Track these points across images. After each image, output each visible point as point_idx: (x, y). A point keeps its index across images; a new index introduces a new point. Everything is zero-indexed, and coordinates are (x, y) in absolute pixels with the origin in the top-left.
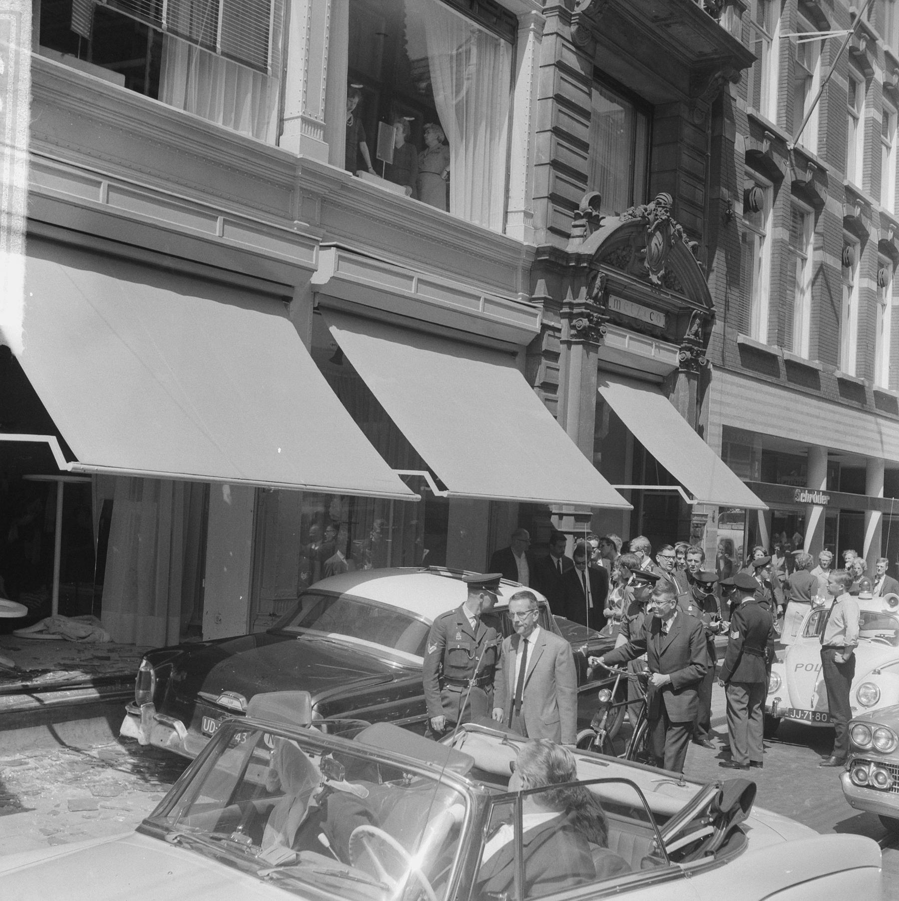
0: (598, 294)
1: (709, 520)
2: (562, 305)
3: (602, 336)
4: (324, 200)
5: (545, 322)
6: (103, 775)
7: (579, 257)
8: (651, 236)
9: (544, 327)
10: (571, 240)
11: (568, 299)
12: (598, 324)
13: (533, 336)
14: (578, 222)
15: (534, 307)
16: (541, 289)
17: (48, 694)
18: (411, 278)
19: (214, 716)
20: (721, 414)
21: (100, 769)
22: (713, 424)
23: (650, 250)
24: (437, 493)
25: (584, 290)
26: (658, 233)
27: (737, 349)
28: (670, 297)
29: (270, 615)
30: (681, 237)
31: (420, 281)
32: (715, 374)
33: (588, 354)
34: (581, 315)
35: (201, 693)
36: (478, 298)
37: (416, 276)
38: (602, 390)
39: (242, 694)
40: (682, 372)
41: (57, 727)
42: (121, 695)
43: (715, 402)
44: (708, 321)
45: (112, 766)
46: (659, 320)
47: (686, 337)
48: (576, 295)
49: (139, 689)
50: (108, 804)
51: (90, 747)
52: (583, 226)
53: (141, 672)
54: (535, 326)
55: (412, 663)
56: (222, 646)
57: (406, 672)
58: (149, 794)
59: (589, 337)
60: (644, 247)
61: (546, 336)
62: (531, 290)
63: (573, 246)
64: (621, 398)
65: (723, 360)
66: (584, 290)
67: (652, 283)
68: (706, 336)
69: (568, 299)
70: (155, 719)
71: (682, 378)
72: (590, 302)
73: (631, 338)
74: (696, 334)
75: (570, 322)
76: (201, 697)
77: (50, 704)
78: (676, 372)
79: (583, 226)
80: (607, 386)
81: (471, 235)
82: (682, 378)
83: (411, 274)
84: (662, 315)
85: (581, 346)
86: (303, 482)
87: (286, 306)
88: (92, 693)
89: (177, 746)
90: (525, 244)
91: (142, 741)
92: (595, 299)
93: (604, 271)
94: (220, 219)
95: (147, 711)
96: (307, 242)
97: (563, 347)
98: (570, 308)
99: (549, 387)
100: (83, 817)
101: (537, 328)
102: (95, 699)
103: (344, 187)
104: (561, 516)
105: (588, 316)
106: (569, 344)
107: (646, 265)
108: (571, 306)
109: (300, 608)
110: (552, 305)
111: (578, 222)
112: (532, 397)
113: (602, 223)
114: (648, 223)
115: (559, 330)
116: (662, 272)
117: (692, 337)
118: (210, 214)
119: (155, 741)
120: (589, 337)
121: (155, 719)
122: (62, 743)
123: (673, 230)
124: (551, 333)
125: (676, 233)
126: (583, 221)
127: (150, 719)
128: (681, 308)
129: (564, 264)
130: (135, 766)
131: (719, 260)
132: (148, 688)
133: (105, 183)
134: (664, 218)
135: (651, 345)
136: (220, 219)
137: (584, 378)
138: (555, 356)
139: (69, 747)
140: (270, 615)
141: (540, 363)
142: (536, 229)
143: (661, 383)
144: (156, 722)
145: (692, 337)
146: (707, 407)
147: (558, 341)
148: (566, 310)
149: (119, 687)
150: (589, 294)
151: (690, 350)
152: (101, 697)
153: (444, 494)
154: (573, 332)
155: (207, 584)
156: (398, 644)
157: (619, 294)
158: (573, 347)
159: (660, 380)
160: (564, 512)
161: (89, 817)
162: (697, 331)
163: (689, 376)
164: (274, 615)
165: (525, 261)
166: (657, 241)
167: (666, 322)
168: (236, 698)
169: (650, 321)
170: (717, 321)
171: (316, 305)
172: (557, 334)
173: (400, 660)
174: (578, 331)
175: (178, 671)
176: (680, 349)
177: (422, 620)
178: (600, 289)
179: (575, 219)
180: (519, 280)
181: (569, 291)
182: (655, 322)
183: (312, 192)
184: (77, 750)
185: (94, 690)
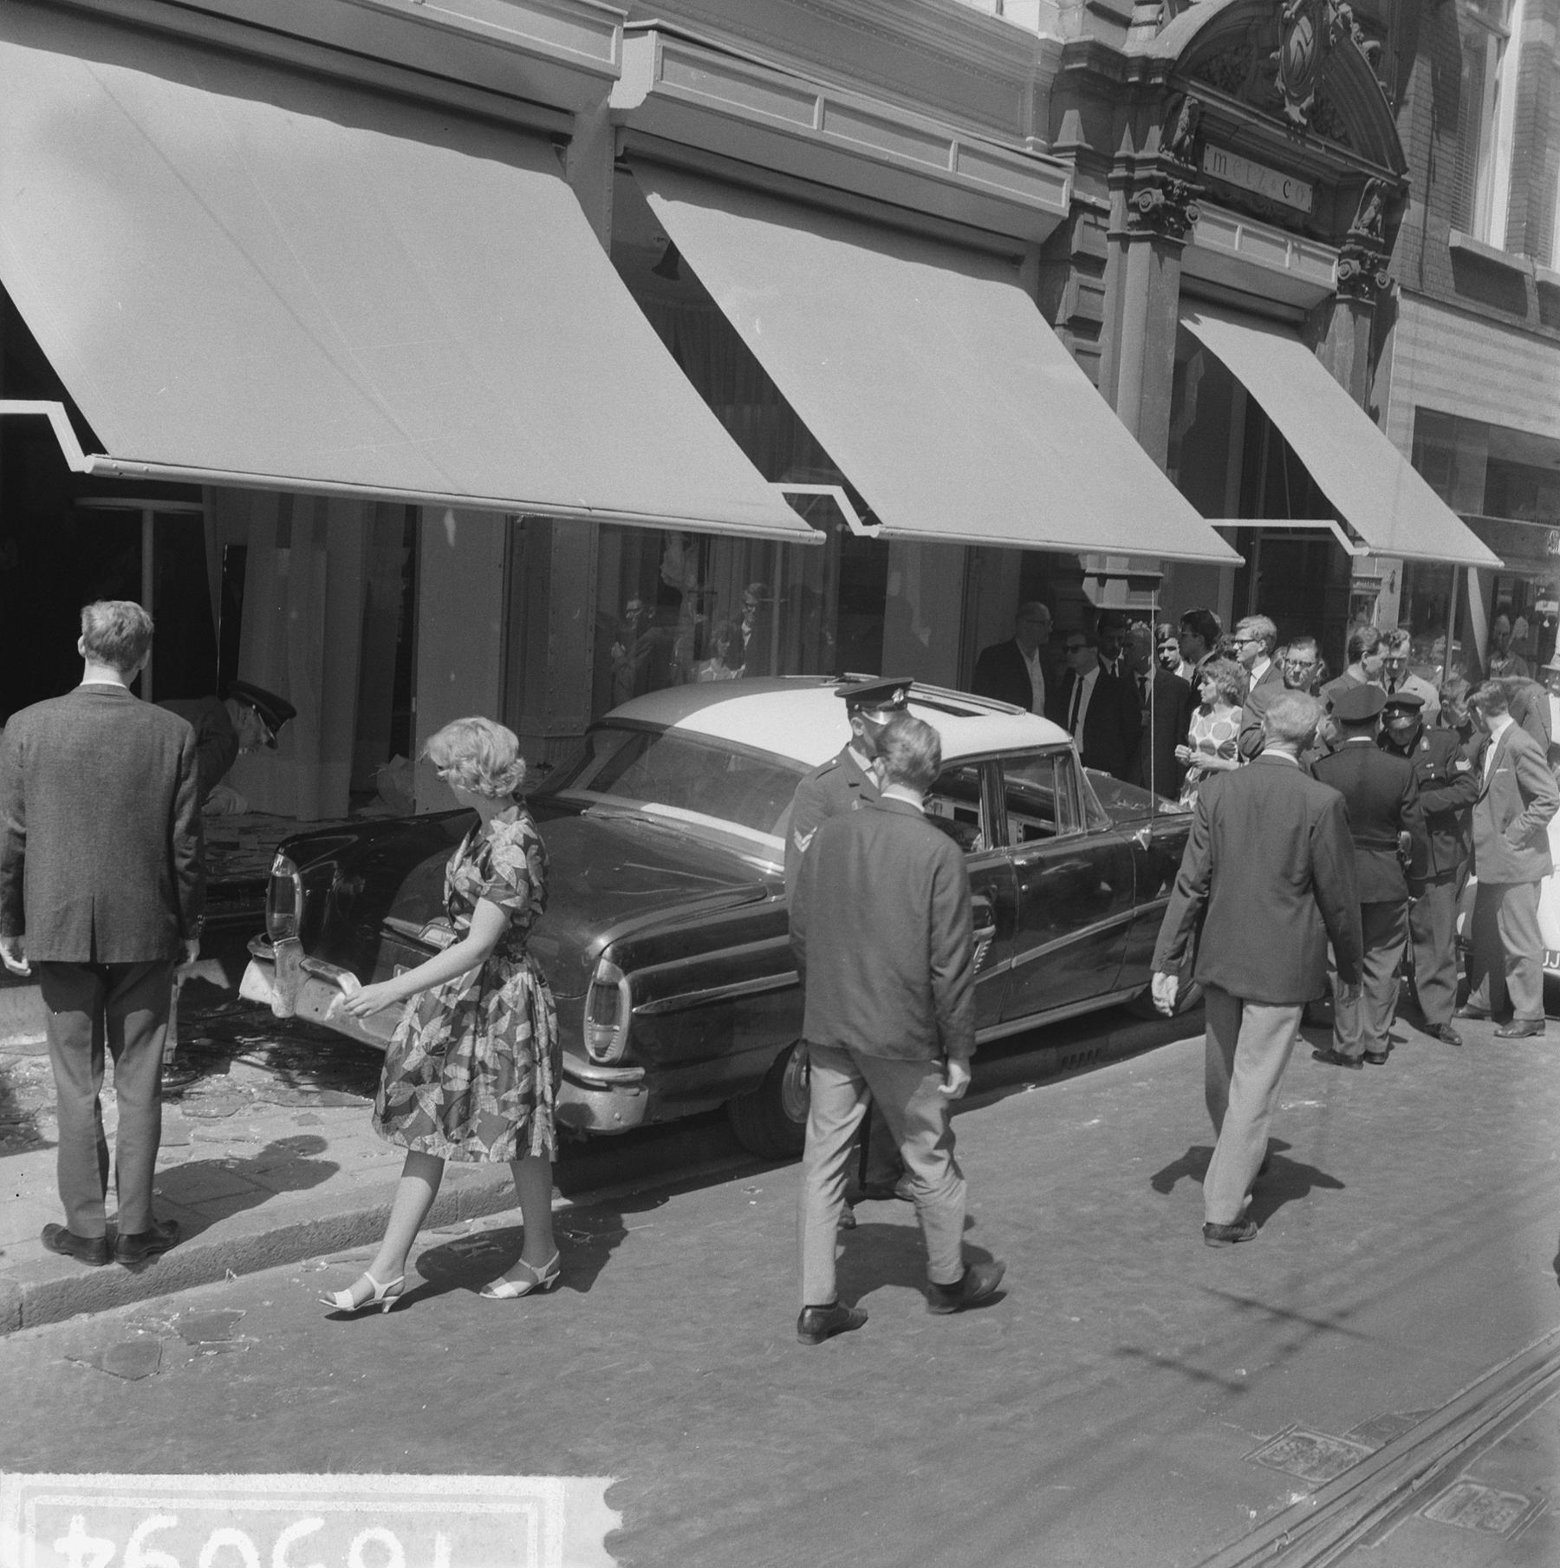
0: (1183, 139)
1: (1384, 589)
2: (1111, 163)
3: (1189, 226)
5: (1079, 195)
7: (1147, 65)
8: (1289, 25)
9: (1077, 206)
10: (1131, 30)
12: (1183, 200)
13: (1052, 226)
16: (1071, 131)
18: (811, 99)
20: (1412, 385)
23: (1288, 52)
24: (857, 527)
25: (1155, 133)
26: (1304, 20)
27: (1448, 258)
28: (1323, 151)
30: (1349, 30)
31: (829, 105)
32: (1405, 306)
33: (1161, 260)
34: (1150, 182)
35: (390, 920)
36: (946, 143)
37: (822, 95)
40: (1341, 301)
43: (1402, 360)
44: (1394, 201)
46: (1300, 198)
47: (1352, 231)
48: (1139, 144)
59: (1164, 228)
60: (1276, 49)
62: (1052, 130)
63: (1136, 43)
66: (1155, 133)
67: (1290, 122)
68: (1391, 230)
71: (1342, 311)
72: (1168, 156)
74: (1372, 226)
75: (1128, 196)
76: (390, 928)
78: (1330, 300)
82: (1342, 311)
83: (811, 89)
84: (1307, 187)
86: (584, 503)
90: (1042, 36)
92: (1178, 150)
93: (1196, 94)
97: (1113, 247)
98: (1127, 169)
99: (1082, 328)
101: (1062, 207)
104: (1102, 579)
105: (1163, 184)
106: (1124, 240)
108: (1130, 163)
110: (1092, 161)
116: (1310, 100)
117: (1364, 232)
119: (304, 1011)
120: (1164, 228)
121: (304, 969)
123: (1332, 14)
125: (1339, 21)
128: (1343, 174)
129: (1118, 78)
132: (288, 907)
135: (1284, 246)
141: (1067, 279)
143: (1301, 321)
144: (304, 976)
148: (1119, 172)
151: (1359, 256)
153: (873, 531)
154: (1133, 216)
158: (1132, 245)
159: (1296, 316)
160: (1108, 571)
163: (1356, 308)
165: (1039, 71)
167: (1314, 202)
169: (1282, 199)
170: (1412, 203)
171: (620, 154)
172: (1101, 221)
174: (1142, 214)
175: (348, 875)
176: (1340, 257)
178: (1188, 131)
181: (1127, 135)
182: (1291, 202)
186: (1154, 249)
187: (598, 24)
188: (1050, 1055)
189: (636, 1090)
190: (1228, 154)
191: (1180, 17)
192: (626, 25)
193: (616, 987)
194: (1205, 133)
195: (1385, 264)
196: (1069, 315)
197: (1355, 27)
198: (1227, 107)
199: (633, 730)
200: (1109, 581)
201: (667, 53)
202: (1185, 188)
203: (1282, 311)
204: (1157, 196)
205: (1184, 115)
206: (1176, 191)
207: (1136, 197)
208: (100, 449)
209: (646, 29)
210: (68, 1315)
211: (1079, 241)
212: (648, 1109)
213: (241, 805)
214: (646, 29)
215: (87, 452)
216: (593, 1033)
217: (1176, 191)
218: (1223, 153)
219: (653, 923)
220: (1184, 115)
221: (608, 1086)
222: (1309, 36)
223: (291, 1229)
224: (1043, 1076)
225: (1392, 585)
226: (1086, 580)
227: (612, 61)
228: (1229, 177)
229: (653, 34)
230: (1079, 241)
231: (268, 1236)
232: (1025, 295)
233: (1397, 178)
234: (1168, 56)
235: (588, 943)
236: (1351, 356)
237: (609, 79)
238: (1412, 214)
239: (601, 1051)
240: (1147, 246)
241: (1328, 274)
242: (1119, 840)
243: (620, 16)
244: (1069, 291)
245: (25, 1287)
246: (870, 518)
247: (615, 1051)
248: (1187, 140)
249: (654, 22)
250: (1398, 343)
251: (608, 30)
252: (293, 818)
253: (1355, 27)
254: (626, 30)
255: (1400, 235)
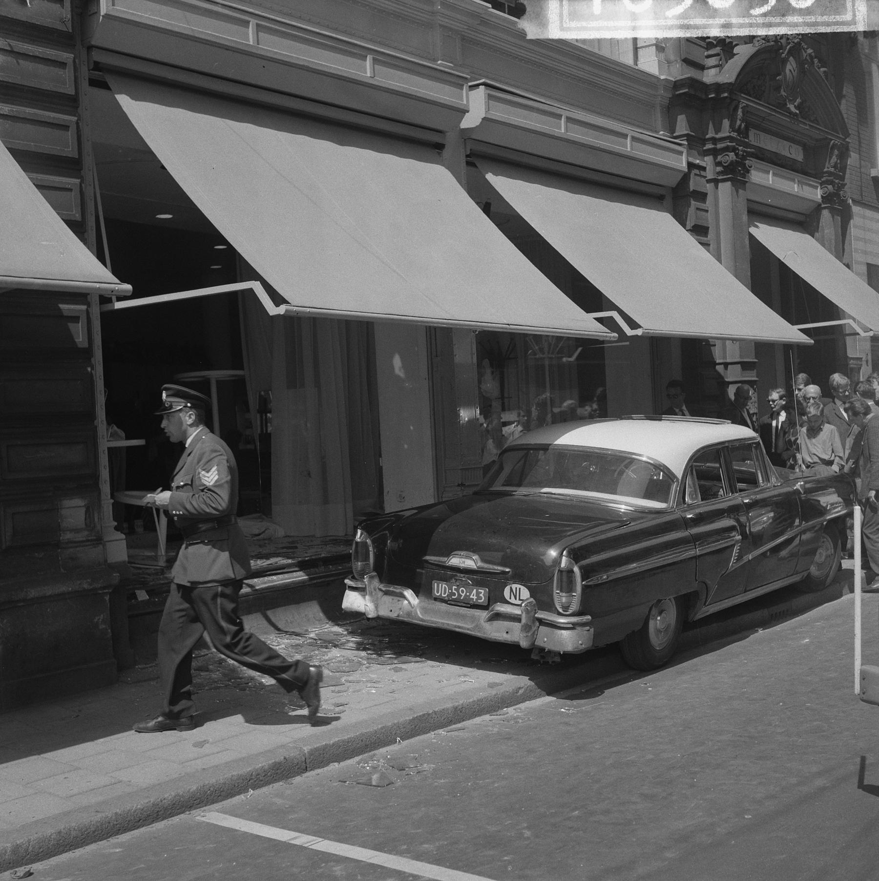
0: (740, 125)
1: (864, 363)
2: (704, 141)
3: (748, 171)
4: (463, 38)
5: (691, 160)
6: (330, 655)
7: (718, 87)
8: (784, 61)
9: (690, 165)
10: (705, 71)
11: (710, 135)
12: (744, 158)
13: (679, 177)
14: (711, 52)
15: (680, 145)
16: (682, 126)
17: (256, 580)
18: (559, 117)
19: (445, 579)
20: (865, 253)
21: (325, 650)
22: (858, 263)
23: (785, 76)
24: (629, 332)
25: (726, 123)
26: (791, 58)
27: (871, 183)
28: (807, 127)
29: (459, 485)
30: (813, 63)
31: (569, 119)
32: (856, 209)
33: (737, 192)
34: (727, 149)
35: (427, 558)
36: (625, 136)
37: (565, 114)
38: (752, 230)
39: (474, 552)
40: (825, 208)
41: (269, 613)
42: (321, 577)
43: (858, 239)
44: (844, 154)
45: (336, 646)
46: (797, 154)
47: (826, 170)
48: (718, 130)
49: (358, 561)
50: (351, 678)
51: (307, 631)
52: (718, 55)
53: (357, 543)
54: (682, 164)
55: (642, 507)
56: (425, 514)
57: (640, 515)
58: (389, 667)
59: (736, 173)
60: (779, 74)
61: (692, 176)
62: (672, 130)
63: (710, 77)
64: (768, 235)
65: (862, 195)
66: (726, 123)
67: (791, 113)
68: (843, 169)
69: (710, 135)
70: (380, 590)
71: (826, 213)
72: (734, 135)
73: (774, 174)
74: (835, 167)
75: (715, 158)
76: (427, 561)
77: (263, 589)
78: (818, 208)
79: (718, 55)
80: (757, 227)
81: (607, 69)
82: (826, 213)
83: (559, 111)
84: (800, 148)
85: (729, 183)
86: (505, 322)
87: (439, 154)
88: (300, 576)
89: (409, 614)
90: (662, 77)
91: (371, 615)
92: (739, 131)
93: (744, 101)
94: (369, 58)
95: (372, 582)
96: (458, 82)
97: (709, 187)
98: (713, 144)
99: (699, 231)
100: (333, 692)
101: (684, 166)
102: (303, 582)
103: (484, 22)
104: (726, 365)
105: (734, 150)
106: (716, 182)
107: (783, 93)
108: (714, 140)
109: (501, 468)
110: (695, 142)
111: (711, 52)
112: (689, 240)
113: (736, 50)
114: (781, 47)
115: (704, 169)
116: (799, 100)
117: (832, 170)
118: (360, 53)
119: (384, 612)
120: (736, 173)
121: (380, 590)
122: (278, 629)
123: (805, 55)
124: (697, 172)
125: (808, 58)
126: (718, 50)
127: (375, 590)
128: (817, 140)
129: (704, 97)
130: (358, 643)
131: (848, 90)
132: (367, 558)
133: (253, 22)
134: (796, 41)
135: (793, 180)
136: (369, 58)
137: (735, 218)
138: (702, 196)
139: (286, 632)
140: (459, 485)
141: (689, 205)
142: (669, 62)
143: (803, 221)
144: (380, 594)
145: (832, 170)
146: (850, 244)
147: (704, 180)
148: (709, 146)
149: (322, 569)
150: (732, 126)
151: (831, 183)
152: (311, 579)
153: (639, 332)
154: (719, 169)
155: (385, 462)
156: (619, 490)
157: (758, 127)
158: (720, 184)
160: (728, 361)
161: (339, 692)
162: (836, 163)
163: (833, 211)
164: (462, 485)
165: (663, 95)
166: (791, 66)
167: (805, 155)
168: (467, 557)
169: (789, 155)
170: (852, 154)
172: (703, 173)
173: (626, 504)
174: (724, 167)
175: (394, 540)
176: (821, 184)
177: (644, 459)
178: (742, 120)
179: (707, 49)
180: (658, 118)
181: (711, 126)
182: (793, 156)
183: (451, 29)
184: (297, 635)
185: (301, 573)
186: (733, 185)
187: (454, 83)
188: (763, 613)
189: (588, 628)
190: (761, 133)
191: (730, 62)
192: (470, 84)
193: (572, 571)
194: (752, 123)
195: (844, 185)
196: (693, 224)
197: (816, 61)
198: (760, 107)
199: (525, 449)
200: (729, 366)
201: (490, 97)
202: (744, 151)
203: (791, 216)
204: (732, 156)
205: (740, 112)
206: (741, 153)
207: (719, 158)
208: (285, 302)
209: (478, 85)
210: (327, 765)
211: (694, 184)
212: (596, 636)
213: (281, 533)
214: (478, 85)
215: (277, 305)
216: (560, 598)
217: (741, 153)
218: (758, 132)
219: (585, 539)
220: (740, 112)
221: (573, 627)
222: (795, 66)
223: (424, 715)
224: (766, 623)
225: (867, 361)
226: (717, 367)
227: (465, 102)
228: (762, 145)
229: (482, 87)
230: (694, 184)
231: (414, 719)
232: (670, 216)
233: (844, 140)
234: (729, 81)
235: (544, 554)
236: (833, 237)
237: (464, 111)
238: (853, 159)
239: (566, 608)
240: (729, 184)
241: (817, 194)
242: (789, 489)
243: (466, 78)
244: (692, 211)
245: (306, 749)
246: (634, 325)
247: (574, 607)
248: (743, 125)
249: (483, 80)
250: (853, 231)
251: (461, 87)
252: (313, 536)
253: (816, 61)
254: (470, 87)
255: (848, 171)
